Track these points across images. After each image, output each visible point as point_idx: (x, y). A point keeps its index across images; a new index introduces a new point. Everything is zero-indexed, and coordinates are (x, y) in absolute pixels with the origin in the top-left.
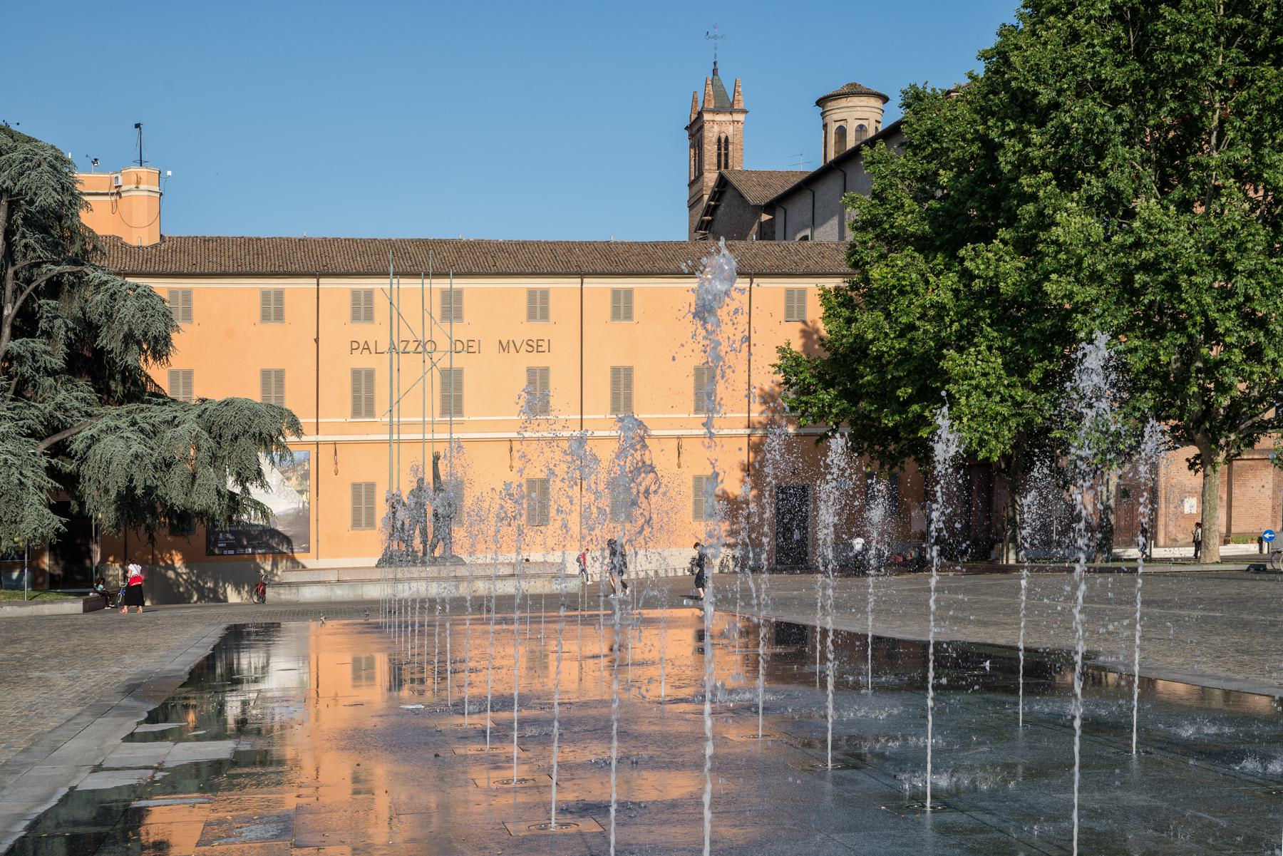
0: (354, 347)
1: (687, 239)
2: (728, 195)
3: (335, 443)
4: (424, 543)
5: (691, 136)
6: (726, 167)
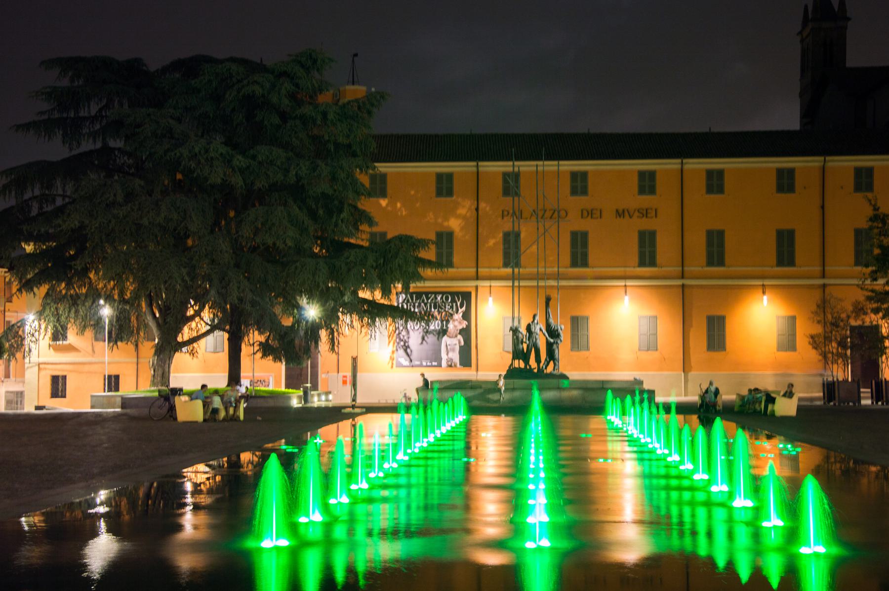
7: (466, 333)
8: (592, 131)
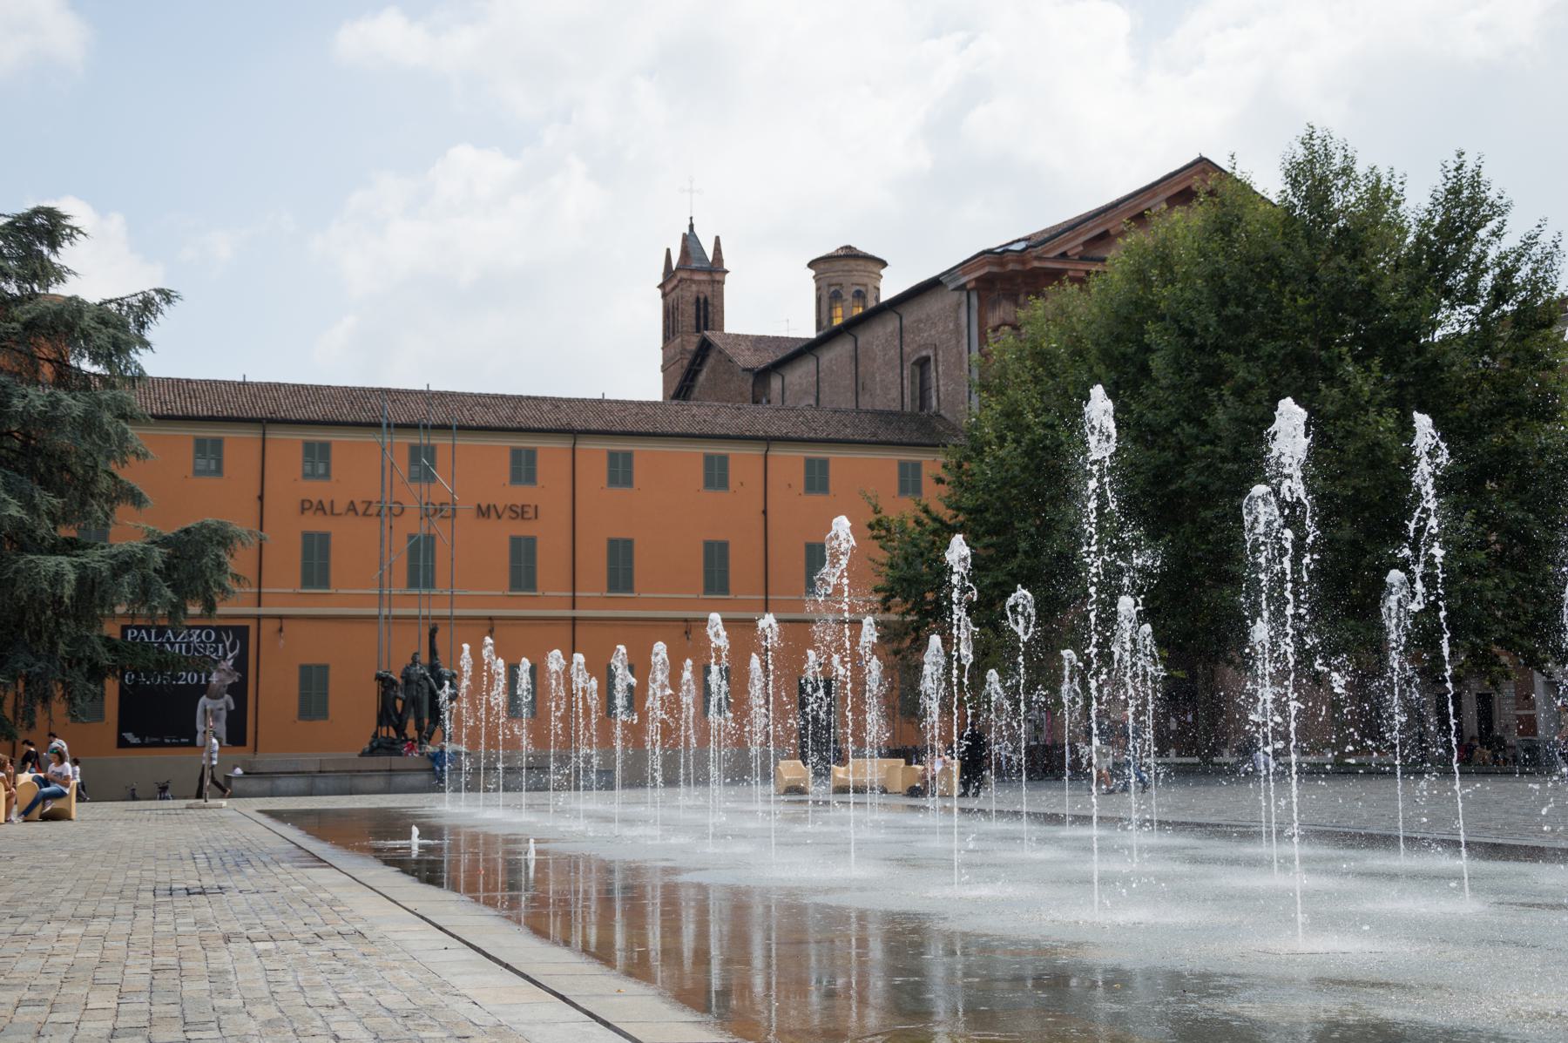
0: (305, 506)
1: (660, 398)
3: (490, 618)
7: (238, 691)
8: (433, 388)
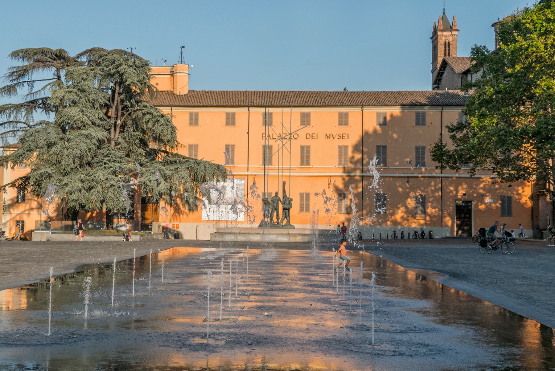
2: (447, 68)
4: (278, 219)
5: (433, 42)
6: (449, 55)
